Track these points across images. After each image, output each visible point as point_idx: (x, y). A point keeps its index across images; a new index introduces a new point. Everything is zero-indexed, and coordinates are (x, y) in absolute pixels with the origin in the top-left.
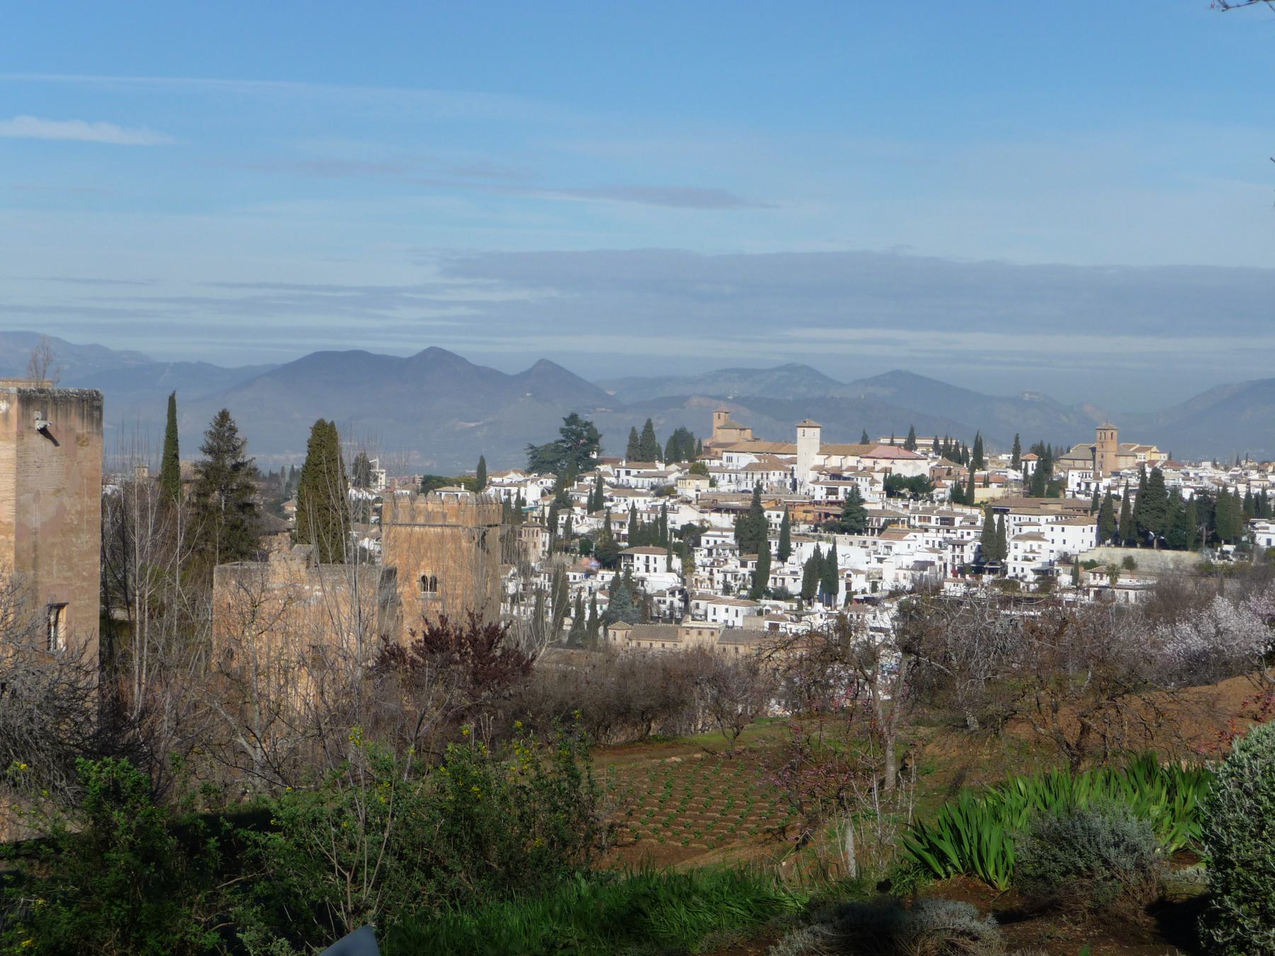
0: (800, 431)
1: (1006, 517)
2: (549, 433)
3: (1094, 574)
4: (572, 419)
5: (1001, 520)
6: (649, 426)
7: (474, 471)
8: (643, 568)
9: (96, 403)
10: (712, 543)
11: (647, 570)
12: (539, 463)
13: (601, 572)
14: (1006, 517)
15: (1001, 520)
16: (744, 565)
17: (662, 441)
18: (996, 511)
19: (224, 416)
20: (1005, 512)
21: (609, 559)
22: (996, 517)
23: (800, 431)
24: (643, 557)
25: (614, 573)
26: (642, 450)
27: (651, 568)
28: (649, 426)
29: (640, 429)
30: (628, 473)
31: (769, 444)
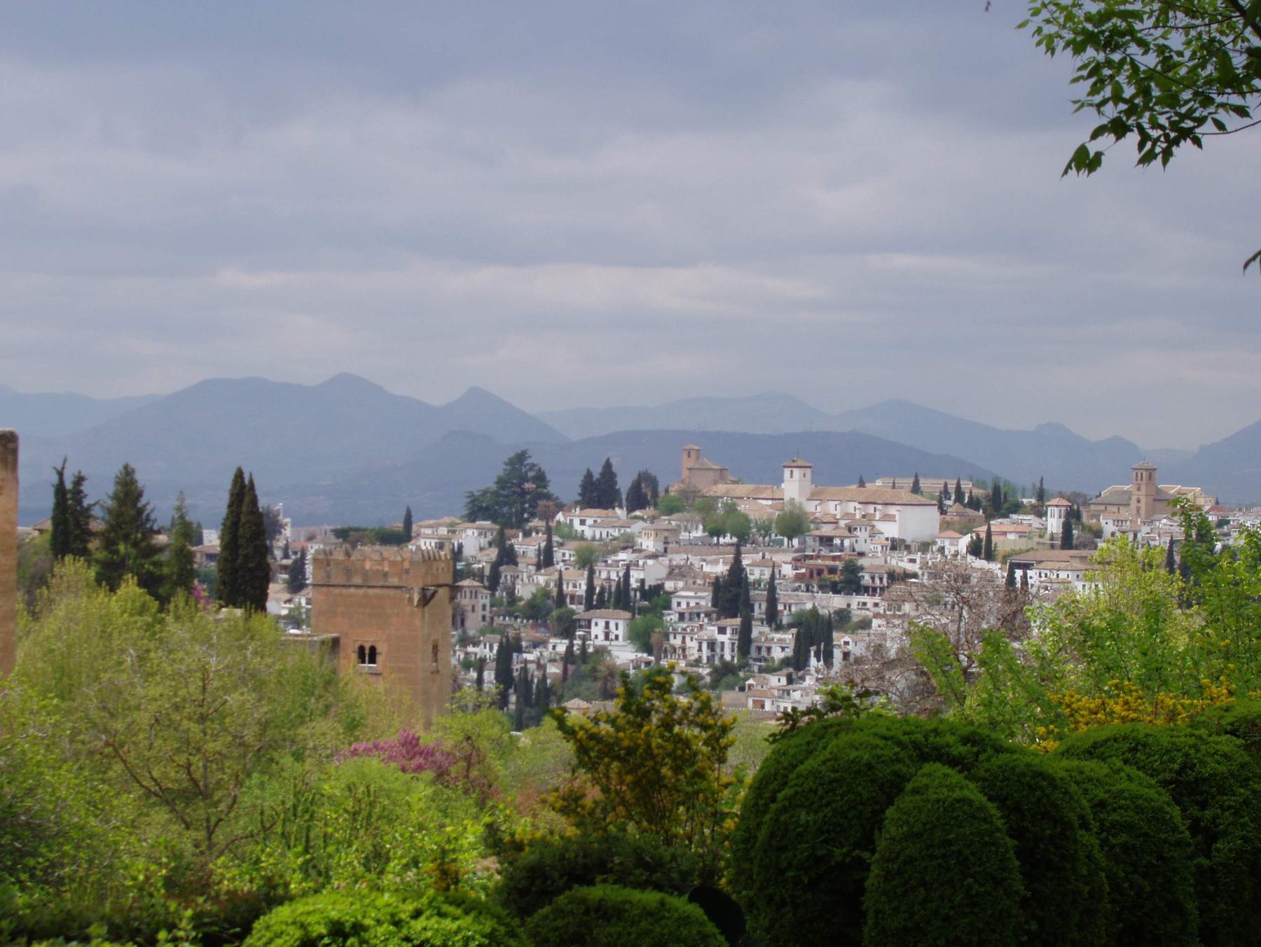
0: (787, 472)
1: (1030, 573)
2: (486, 478)
3: (601, 539)
4: (521, 457)
5: (1025, 577)
6: (608, 465)
7: (401, 525)
8: (601, 637)
9: (11, 445)
10: (684, 606)
11: (607, 637)
12: (477, 510)
13: (553, 641)
14: (1030, 573)
15: (1025, 577)
16: (722, 631)
17: (624, 484)
18: (1019, 566)
19: (239, 475)
20: (1026, 567)
21: (567, 628)
22: (1019, 573)
23: (787, 472)
24: (602, 623)
25: (566, 641)
26: (599, 492)
27: (612, 636)
28: (608, 465)
29: (597, 472)
30: (583, 522)
31: (752, 487)
